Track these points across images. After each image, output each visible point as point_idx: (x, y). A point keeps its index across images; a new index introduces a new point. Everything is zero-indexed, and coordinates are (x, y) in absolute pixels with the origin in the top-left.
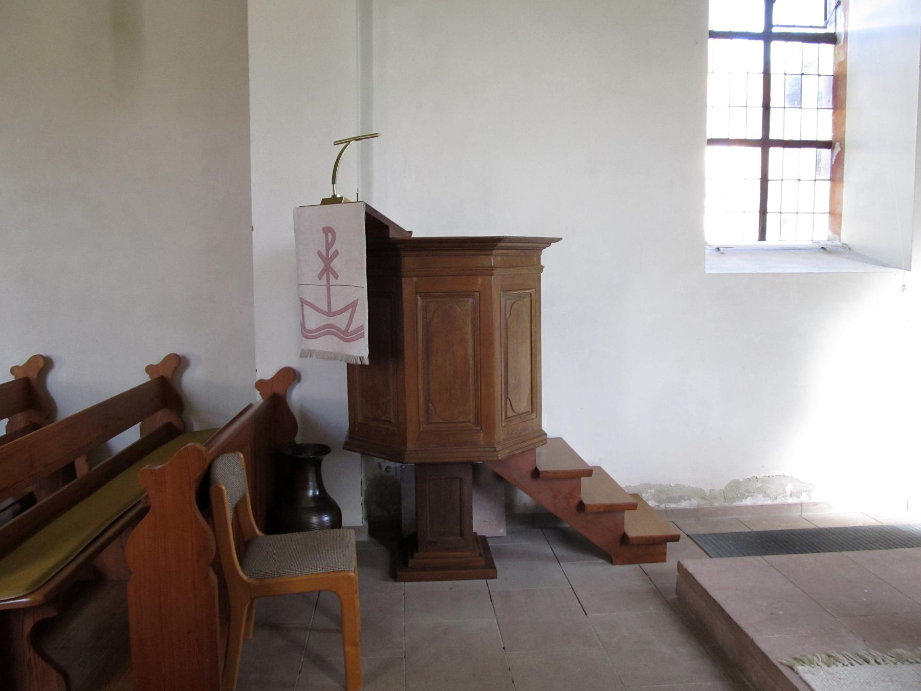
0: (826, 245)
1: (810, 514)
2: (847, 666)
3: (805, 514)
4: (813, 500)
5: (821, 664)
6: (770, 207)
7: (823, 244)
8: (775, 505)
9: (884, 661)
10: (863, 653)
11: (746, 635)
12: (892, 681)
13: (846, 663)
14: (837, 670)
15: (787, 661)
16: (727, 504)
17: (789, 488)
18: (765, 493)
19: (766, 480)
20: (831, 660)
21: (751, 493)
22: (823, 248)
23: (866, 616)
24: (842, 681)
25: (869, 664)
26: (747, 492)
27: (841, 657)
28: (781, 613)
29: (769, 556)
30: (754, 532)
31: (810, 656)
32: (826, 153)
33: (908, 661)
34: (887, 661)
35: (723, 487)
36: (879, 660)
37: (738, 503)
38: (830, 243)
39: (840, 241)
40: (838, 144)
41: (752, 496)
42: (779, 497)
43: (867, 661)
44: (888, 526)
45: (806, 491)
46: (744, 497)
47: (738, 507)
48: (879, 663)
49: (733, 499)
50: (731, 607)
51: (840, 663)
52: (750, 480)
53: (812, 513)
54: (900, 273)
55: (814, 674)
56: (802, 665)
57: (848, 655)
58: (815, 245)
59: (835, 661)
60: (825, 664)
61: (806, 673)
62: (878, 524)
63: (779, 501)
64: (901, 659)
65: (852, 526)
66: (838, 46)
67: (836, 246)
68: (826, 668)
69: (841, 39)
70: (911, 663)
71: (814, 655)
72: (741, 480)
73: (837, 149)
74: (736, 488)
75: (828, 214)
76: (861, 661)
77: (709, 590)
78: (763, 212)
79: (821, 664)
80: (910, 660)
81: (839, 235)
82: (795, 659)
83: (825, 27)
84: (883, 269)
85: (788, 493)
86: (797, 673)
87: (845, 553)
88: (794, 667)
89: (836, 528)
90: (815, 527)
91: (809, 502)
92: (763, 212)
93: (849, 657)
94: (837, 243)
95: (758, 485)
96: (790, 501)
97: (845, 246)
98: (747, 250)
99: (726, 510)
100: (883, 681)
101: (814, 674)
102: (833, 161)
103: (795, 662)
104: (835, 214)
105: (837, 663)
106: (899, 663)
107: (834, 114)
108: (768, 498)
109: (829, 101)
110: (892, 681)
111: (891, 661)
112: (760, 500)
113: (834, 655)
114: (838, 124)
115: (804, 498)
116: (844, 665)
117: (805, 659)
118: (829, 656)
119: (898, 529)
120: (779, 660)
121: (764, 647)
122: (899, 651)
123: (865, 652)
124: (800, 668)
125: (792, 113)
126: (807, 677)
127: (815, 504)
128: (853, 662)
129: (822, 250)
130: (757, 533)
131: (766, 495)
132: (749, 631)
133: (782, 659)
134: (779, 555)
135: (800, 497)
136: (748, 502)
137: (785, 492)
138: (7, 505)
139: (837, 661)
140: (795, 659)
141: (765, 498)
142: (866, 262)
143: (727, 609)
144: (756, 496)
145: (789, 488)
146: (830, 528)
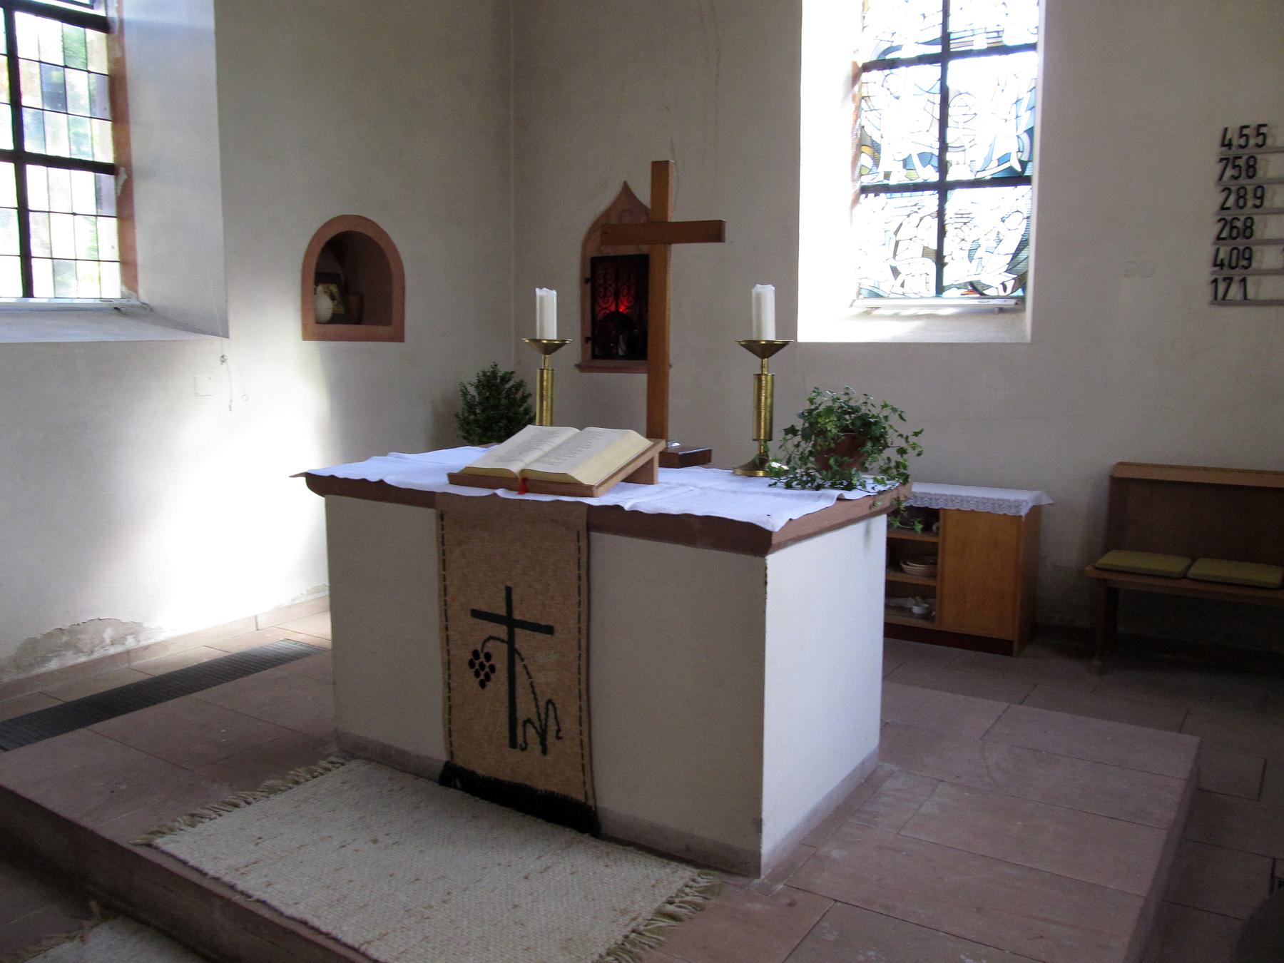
0: (122, 305)
1: (140, 662)
2: (215, 818)
3: (136, 664)
4: (143, 643)
5: (184, 827)
6: (35, 249)
7: (116, 304)
8: (91, 661)
9: (255, 799)
10: (231, 798)
11: (84, 829)
12: (267, 816)
13: (214, 816)
14: (204, 827)
15: (143, 839)
16: (22, 676)
17: (108, 634)
18: (75, 647)
19: (72, 631)
20: (195, 819)
21: (57, 651)
22: (116, 308)
23: (227, 758)
24: (212, 837)
25: (238, 807)
26: (50, 653)
27: (206, 812)
28: (124, 787)
29: (96, 725)
30: (68, 703)
31: (170, 824)
32: (107, 179)
33: (280, 790)
34: (259, 798)
35: (12, 652)
36: (250, 799)
37: (42, 670)
38: (125, 302)
39: (138, 300)
40: (122, 170)
41: (57, 656)
42: (96, 649)
43: (237, 806)
44: (237, 654)
45: (131, 634)
46: (46, 659)
47: (38, 677)
48: (249, 803)
49: (32, 666)
50: (55, 802)
51: (206, 818)
52: (52, 634)
53: (144, 661)
54: (217, 341)
55: (178, 842)
56: (162, 837)
57: (214, 807)
58: (105, 305)
59: (200, 819)
60: (190, 825)
61: (169, 843)
62: (227, 654)
63: (96, 655)
64: (273, 791)
65: (195, 664)
66: (111, 36)
67: (133, 306)
68: (190, 829)
69: (116, 28)
70: (284, 791)
71: (175, 821)
72: (39, 637)
73: (123, 177)
74: (35, 649)
75: (117, 264)
76: (229, 808)
77: (22, 791)
78: (26, 256)
79: (184, 827)
80: (283, 788)
81: (136, 291)
82: (152, 833)
83: (92, 7)
84: (202, 336)
85: (108, 641)
86: (156, 848)
87: (195, 695)
88: (152, 843)
89: (176, 672)
90: (151, 677)
91: (138, 646)
92: (26, 256)
93: (216, 808)
94: (134, 302)
95: (65, 638)
96: (112, 651)
97: (145, 306)
98: (8, 310)
99: (19, 686)
100: (258, 820)
101: (178, 842)
102: (119, 192)
103: (150, 836)
104: (127, 263)
105: (203, 820)
106: (271, 796)
107: (114, 129)
108: (81, 654)
109: (105, 109)
110: (267, 816)
111: (263, 796)
112: (72, 659)
113: (197, 812)
114: (121, 141)
115: (130, 643)
116: (211, 819)
117: (164, 829)
118: (192, 815)
119: (250, 654)
120: (133, 842)
121: (109, 833)
122: (269, 782)
123: (232, 797)
124: (159, 842)
125: (55, 120)
126: (170, 848)
127: (146, 648)
128: (222, 812)
129: (115, 311)
130: (72, 703)
131: (79, 651)
132: (87, 822)
133: (135, 839)
134: (506, 442)
135: (124, 644)
136: (53, 665)
137: (103, 640)
138: (631, 466)
139: (202, 817)
140: (152, 833)
141: (76, 656)
142: (177, 328)
143: (51, 805)
144: (64, 655)
145: (108, 634)
146: (169, 673)
